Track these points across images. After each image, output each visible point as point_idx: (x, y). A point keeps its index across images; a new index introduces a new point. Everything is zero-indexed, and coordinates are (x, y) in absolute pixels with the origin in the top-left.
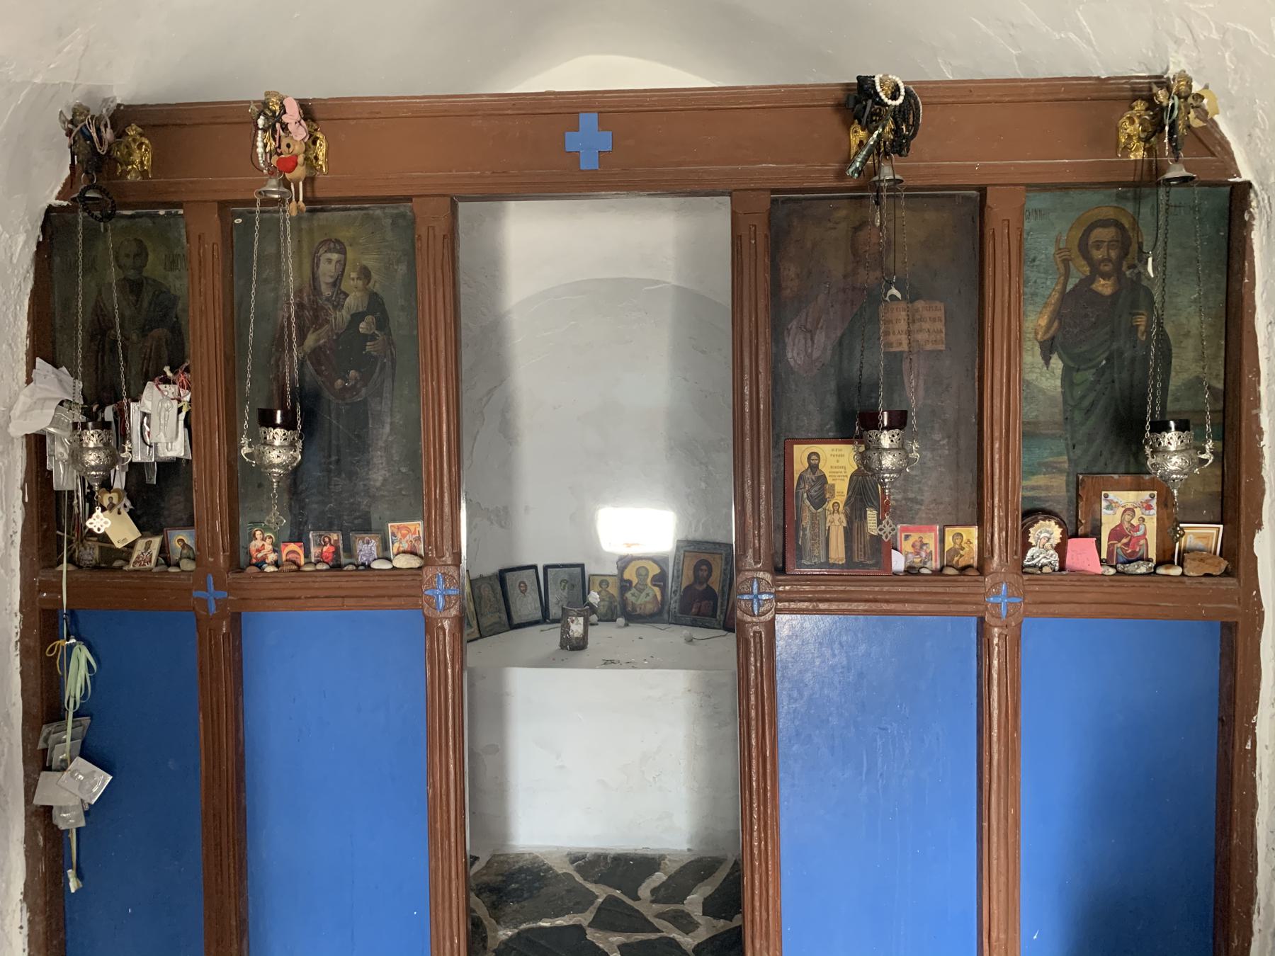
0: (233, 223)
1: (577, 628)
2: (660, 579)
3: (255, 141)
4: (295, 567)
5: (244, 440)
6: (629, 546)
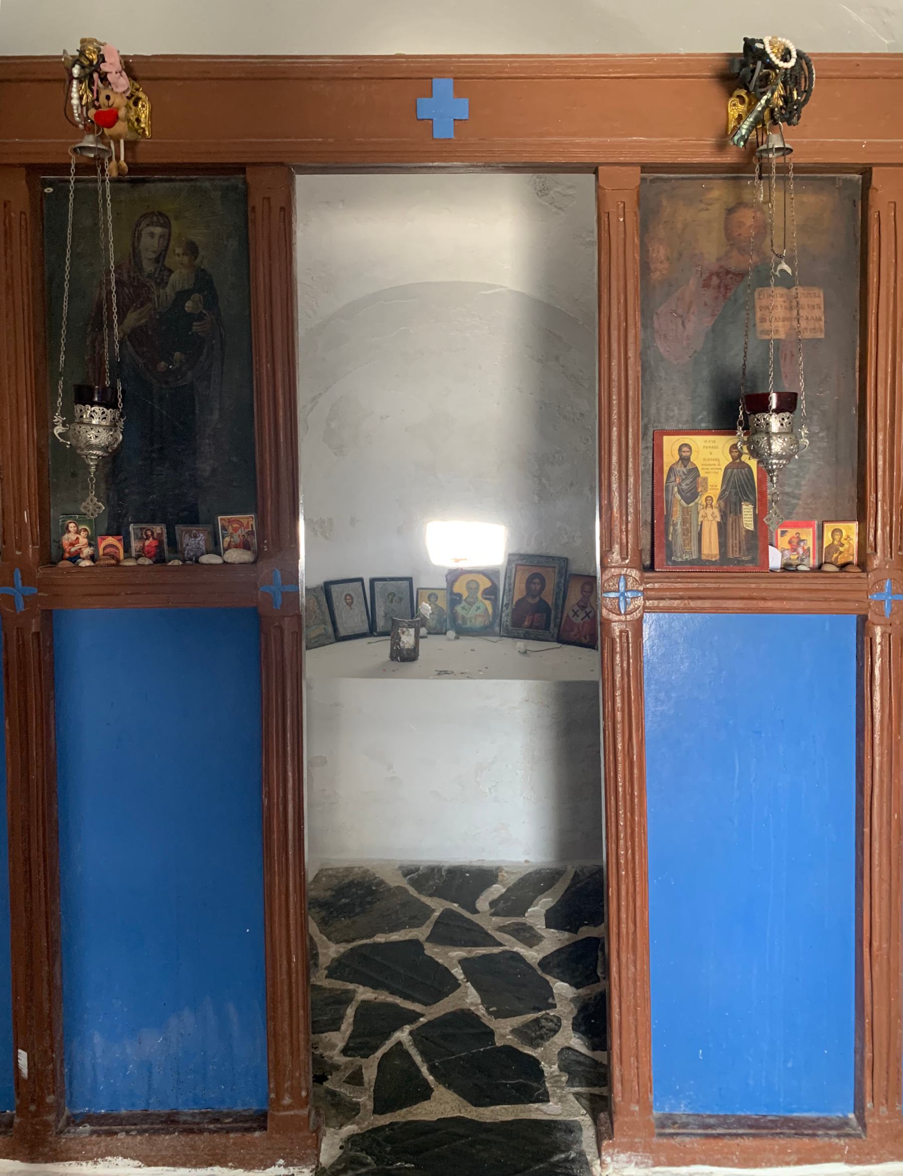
0: (42, 192)
1: (407, 639)
2: (491, 592)
3: (69, 91)
4: (113, 562)
5: (58, 418)
6: (457, 561)
